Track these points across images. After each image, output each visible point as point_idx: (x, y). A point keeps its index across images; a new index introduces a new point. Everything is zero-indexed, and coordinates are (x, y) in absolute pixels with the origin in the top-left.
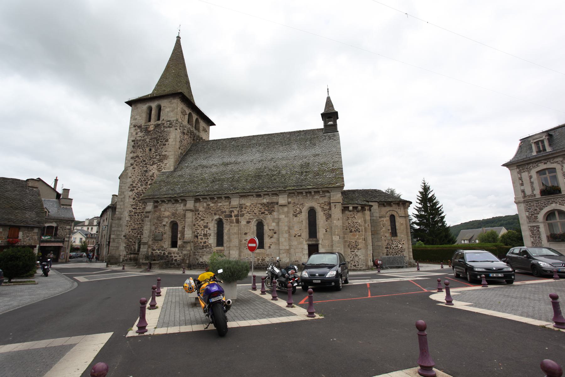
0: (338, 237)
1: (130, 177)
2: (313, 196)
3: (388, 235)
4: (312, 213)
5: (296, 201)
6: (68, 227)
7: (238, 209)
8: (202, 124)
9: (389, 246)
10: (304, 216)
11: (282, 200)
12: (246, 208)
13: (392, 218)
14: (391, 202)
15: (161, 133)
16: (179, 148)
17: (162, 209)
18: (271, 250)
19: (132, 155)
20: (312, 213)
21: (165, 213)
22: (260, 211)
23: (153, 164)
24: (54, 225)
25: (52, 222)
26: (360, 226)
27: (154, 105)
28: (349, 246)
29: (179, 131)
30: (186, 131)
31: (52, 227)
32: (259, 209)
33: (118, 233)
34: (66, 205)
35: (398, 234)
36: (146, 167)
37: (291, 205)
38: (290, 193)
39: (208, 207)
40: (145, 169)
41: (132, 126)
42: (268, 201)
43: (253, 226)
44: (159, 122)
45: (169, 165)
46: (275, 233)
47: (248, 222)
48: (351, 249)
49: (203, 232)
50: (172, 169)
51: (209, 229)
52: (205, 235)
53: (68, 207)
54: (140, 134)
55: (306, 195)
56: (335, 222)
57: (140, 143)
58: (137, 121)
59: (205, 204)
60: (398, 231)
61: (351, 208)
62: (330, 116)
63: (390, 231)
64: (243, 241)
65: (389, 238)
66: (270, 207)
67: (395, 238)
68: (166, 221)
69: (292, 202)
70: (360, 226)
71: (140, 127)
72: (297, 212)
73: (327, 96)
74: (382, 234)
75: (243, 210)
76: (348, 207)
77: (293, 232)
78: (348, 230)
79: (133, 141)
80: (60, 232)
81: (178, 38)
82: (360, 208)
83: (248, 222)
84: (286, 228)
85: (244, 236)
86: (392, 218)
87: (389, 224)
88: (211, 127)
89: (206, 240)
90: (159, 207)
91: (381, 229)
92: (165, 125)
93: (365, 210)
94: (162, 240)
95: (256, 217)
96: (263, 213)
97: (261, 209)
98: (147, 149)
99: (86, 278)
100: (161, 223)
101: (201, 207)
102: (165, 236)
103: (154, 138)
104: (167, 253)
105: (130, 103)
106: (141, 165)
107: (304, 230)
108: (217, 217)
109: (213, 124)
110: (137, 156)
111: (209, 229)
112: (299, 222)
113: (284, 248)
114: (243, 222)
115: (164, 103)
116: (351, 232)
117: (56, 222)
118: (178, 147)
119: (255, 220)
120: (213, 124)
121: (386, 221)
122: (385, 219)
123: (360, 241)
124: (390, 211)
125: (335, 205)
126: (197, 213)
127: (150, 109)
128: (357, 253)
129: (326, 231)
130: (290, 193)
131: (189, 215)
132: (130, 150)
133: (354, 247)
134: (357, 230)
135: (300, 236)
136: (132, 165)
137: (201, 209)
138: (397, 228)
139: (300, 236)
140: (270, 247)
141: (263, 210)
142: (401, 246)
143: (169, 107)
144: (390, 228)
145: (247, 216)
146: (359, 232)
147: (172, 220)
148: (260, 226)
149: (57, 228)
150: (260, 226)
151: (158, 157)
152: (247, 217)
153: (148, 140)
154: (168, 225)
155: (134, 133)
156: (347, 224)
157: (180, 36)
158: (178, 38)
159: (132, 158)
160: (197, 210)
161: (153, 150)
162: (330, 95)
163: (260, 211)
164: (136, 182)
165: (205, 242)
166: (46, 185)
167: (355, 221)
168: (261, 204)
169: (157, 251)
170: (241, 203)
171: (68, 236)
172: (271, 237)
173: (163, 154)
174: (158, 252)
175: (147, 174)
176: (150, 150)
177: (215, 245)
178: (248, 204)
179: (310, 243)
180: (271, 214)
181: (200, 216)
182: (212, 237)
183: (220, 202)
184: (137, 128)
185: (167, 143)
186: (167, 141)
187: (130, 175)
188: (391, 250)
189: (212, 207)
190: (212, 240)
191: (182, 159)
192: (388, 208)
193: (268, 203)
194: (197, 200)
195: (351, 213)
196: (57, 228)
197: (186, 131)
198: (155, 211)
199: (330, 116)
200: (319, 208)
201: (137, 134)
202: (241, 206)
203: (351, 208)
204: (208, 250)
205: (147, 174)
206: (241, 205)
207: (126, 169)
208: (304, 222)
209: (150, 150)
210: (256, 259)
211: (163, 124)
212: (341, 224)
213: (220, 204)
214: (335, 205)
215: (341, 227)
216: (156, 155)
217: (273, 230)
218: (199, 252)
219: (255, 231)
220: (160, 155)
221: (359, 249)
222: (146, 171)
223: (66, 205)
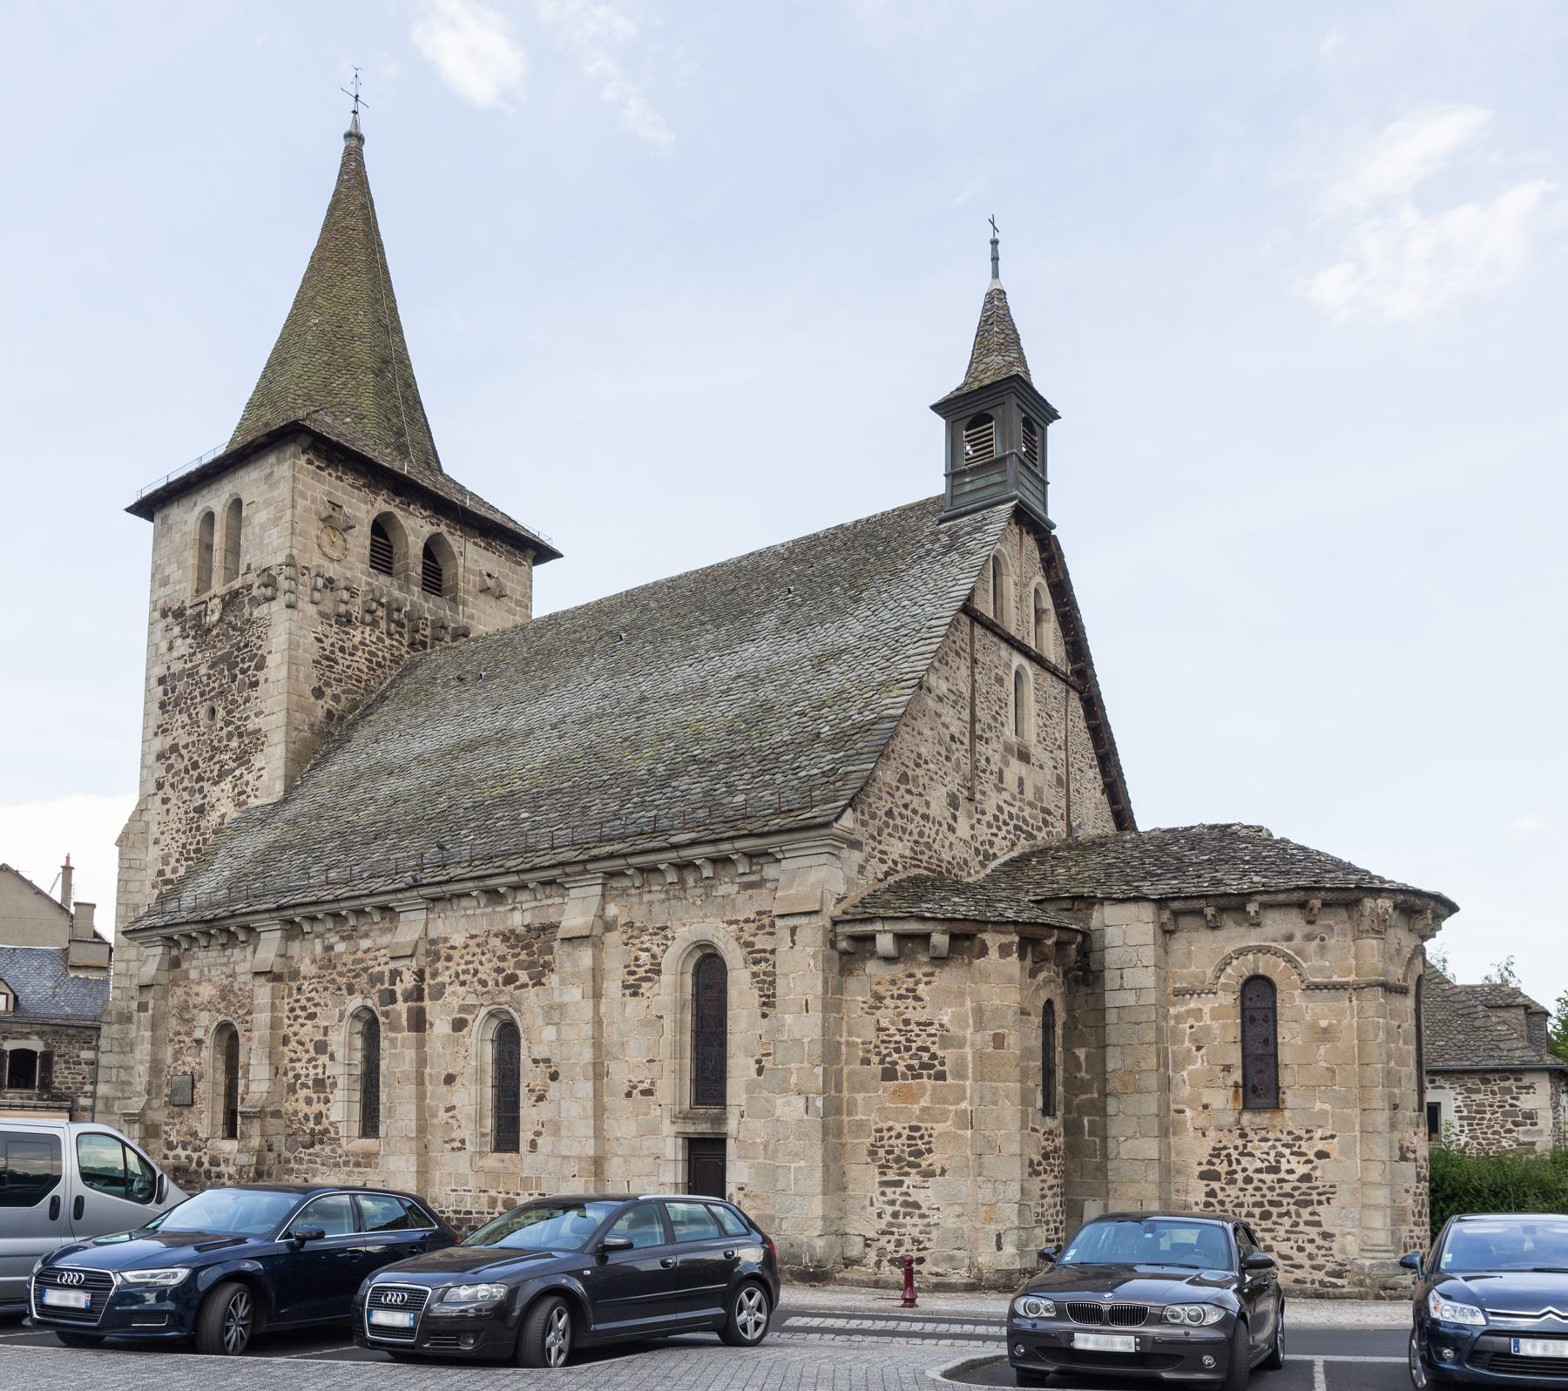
0: (800, 1102)
1: (156, 842)
2: (708, 884)
3: (1222, 1099)
4: (709, 970)
5: (639, 915)
6: (87, 1055)
7: (414, 964)
8: (472, 559)
9: (1222, 1168)
10: (671, 990)
11: (576, 910)
12: (449, 958)
13: (1258, 1000)
14: (1247, 896)
15: (242, 631)
16: (318, 693)
17: (194, 975)
18: (538, 1157)
19: (160, 744)
20: (709, 970)
21: (200, 989)
22: (499, 970)
23: (222, 775)
24: (36, 1045)
25: (26, 1036)
26: (946, 1042)
27: (216, 500)
28: (873, 1153)
29: (312, 610)
30: (356, 610)
31: (31, 1054)
32: (497, 963)
33: (123, 1076)
34: (87, 967)
35: (1290, 1098)
36: (201, 790)
37: (614, 938)
38: (611, 875)
39: (328, 962)
40: (198, 800)
41: (157, 615)
42: (528, 918)
43: (479, 1047)
44: (237, 584)
45: (271, 766)
46: (554, 1077)
47: (459, 1025)
48: (884, 1168)
49: (312, 1072)
50: (279, 789)
51: (332, 1058)
52: (319, 1084)
53: (95, 976)
54: (182, 647)
55: (682, 881)
56: (788, 1018)
57: (180, 686)
58: (169, 589)
59: (319, 949)
60: (1285, 1078)
61: (885, 943)
62: (997, 415)
63: (1237, 1076)
64: (441, 1112)
65: (1230, 1118)
66: (535, 949)
67: (1264, 1119)
68: (206, 1023)
69: (622, 921)
70: (946, 1042)
71: (179, 614)
72: (641, 972)
73: (985, 284)
74: (1186, 1091)
75: (440, 965)
76: (871, 938)
77: (621, 1074)
78: (876, 1068)
79: (162, 681)
80: (62, 1076)
81: (355, 139)
82: (940, 940)
83: (459, 1025)
84: (587, 1055)
85: (443, 1089)
86: (1258, 1000)
87: (1235, 1031)
88: (538, 570)
89: (322, 1107)
90: (185, 965)
91: (1187, 1059)
92: (255, 592)
93: (983, 951)
94: (193, 1103)
95: (486, 1000)
96: (510, 979)
97: (502, 958)
98: (203, 711)
99: (451, 1256)
100: (189, 1034)
101: (306, 956)
102: (201, 1087)
103: (222, 659)
104: (205, 1160)
105: (147, 507)
106: (186, 783)
107: (669, 1064)
108: (355, 1003)
109: (544, 553)
110: (174, 748)
111: (332, 1058)
112: (646, 1023)
113: (575, 1149)
114: (440, 1026)
115: (248, 483)
116: (889, 1074)
117: (41, 1034)
118: (308, 690)
119: (483, 1012)
120: (544, 553)
121: (1215, 1018)
122: (1206, 1004)
123: (939, 1128)
124: (1241, 952)
125: (793, 930)
126: (294, 985)
127: (209, 517)
128: (916, 1196)
129: (760, 1071)
130: (611, 875)
131: (263, 993)
132: (153, 725)
133: (907, 1157)
134: (931, 1068)
135: (647, 1093)
136: (160, 786)
137: (307, 968)
138: (1285, 1055)
139: (647, 1093)
140: (533, 1145)
141: (509, 966)
142: (1302, 1169)
143: (267, 503)
144: (1235, 1056)
145: (456, 996)
146: (941, 1076)
147: (221, 1018)
148: (508, 1036)
149: (47, 1057)
150: (508, 1036)
151: (234, 744)
152: (456, 1003)
153: (203, 670)
154: (209, 1042)
155: (164, 646)
156: (871, 1035)
157: (363, 131)
158: (355, 139)
159: (161, 756)
160: (295, 975)
161: (221, 713)
162: (1005, 283)
163: (499, 970)
164: (172, 862)
165: (319, 1117)
166: (31, 893)
167: (916, 1015)
168: (506, 939)
169: (179, 1151)
170: (432, 935)
171: (88, 1088)
172: (541, 1098)
173: (251, 727)
174: (183, 1154)
175: (203, 824)
176: (213, 712)
177: (356, 1128)
178: (458, 939)
179: (690, 1129)
180: (539, 983)
181: (303, 1002)
182: (339, 1095)
183: (366, 935)
184: (170, 619)
185: (261, 675)
186: (260, 667)
187: (154, 830)
188: (1233, 1191)
189: (340, 955)
190: (342, 1110)
191: (320, 742)
192: (1233, 936)
193: (529, 928)
194: (292, 930)
195: (898, 970)
196: (47, 1057)
197: (356, 610)
198: (174, 982)
199: (997, 415)
200: (733, 945)
201: (170, 648)
202: (434, 950)
203: (885, 943)
204: (328, 1149)
205: (203, 824)
206: (433, 942)
207: (141, 810)
208: (668, 1022)
209: (213, 712)
210: (484, 1198)
211: (249, 587)
212: (817, 1033)
213: (365, 944)
214: (793, 930)
215: (818, 1050)
216: (230, 736)
217: (547, 1061)
218: (300, 1161)
219: (489, 1068)
220: (240, 735)
221: (928, 1174)
222: (200, 810)
223: (87, 967)
